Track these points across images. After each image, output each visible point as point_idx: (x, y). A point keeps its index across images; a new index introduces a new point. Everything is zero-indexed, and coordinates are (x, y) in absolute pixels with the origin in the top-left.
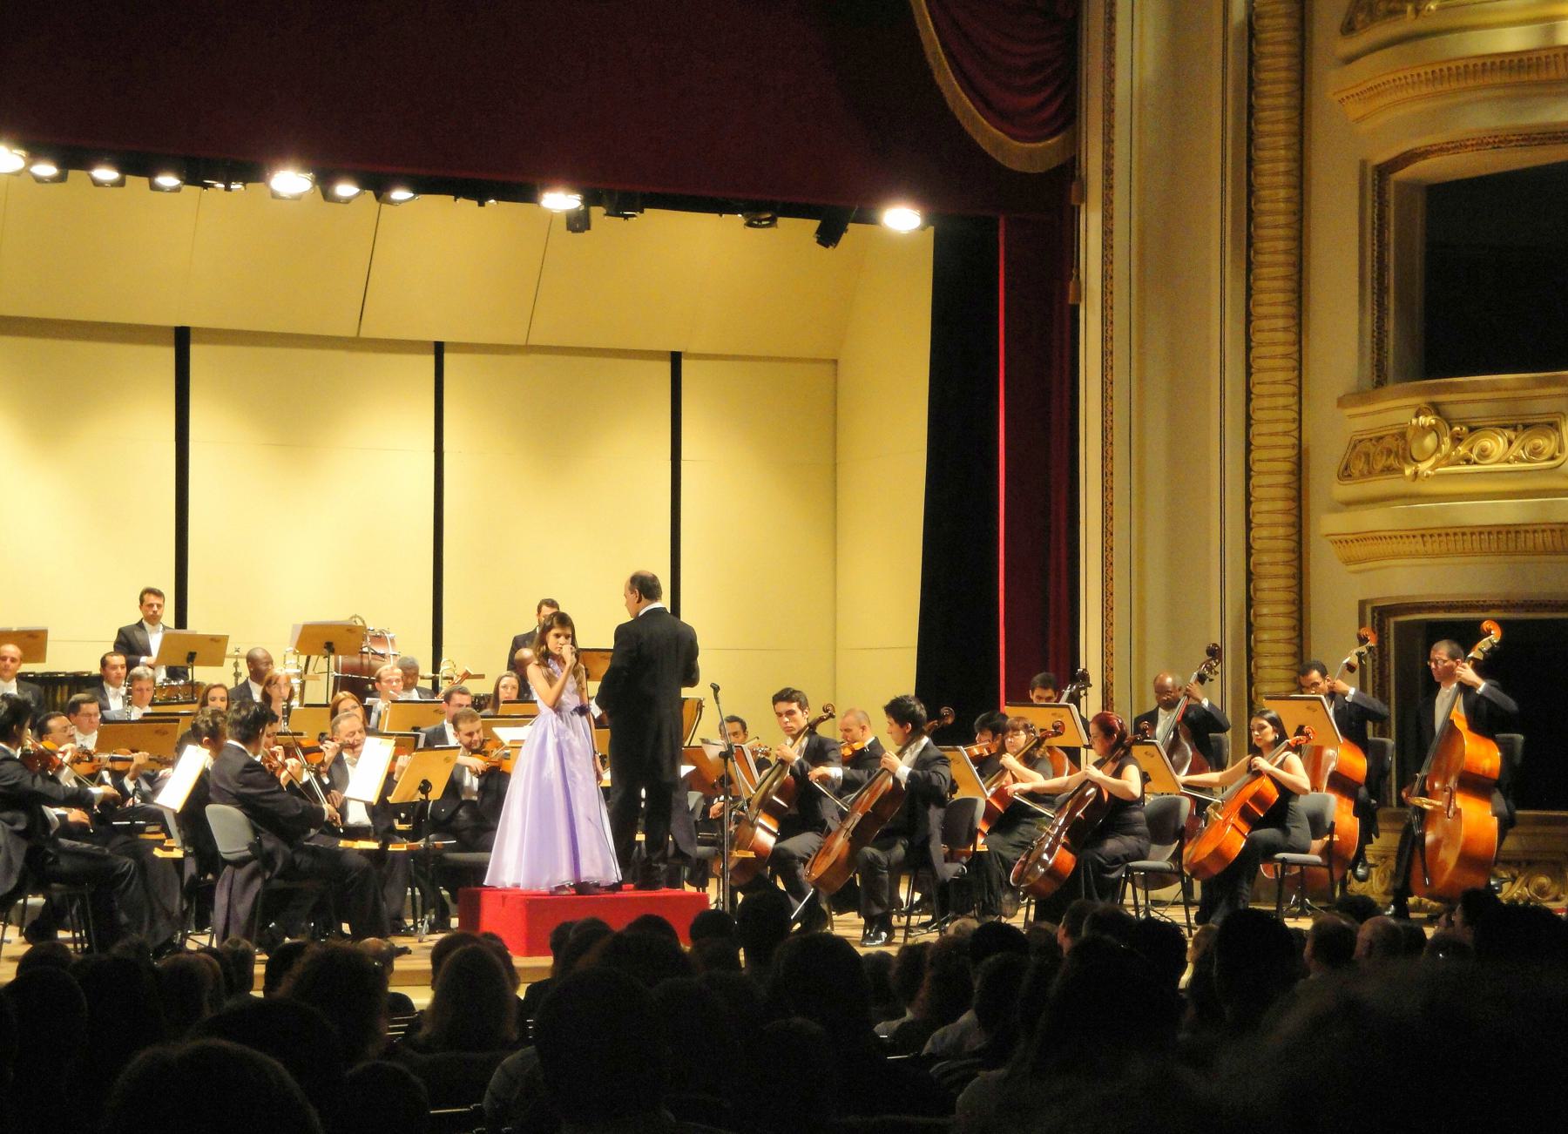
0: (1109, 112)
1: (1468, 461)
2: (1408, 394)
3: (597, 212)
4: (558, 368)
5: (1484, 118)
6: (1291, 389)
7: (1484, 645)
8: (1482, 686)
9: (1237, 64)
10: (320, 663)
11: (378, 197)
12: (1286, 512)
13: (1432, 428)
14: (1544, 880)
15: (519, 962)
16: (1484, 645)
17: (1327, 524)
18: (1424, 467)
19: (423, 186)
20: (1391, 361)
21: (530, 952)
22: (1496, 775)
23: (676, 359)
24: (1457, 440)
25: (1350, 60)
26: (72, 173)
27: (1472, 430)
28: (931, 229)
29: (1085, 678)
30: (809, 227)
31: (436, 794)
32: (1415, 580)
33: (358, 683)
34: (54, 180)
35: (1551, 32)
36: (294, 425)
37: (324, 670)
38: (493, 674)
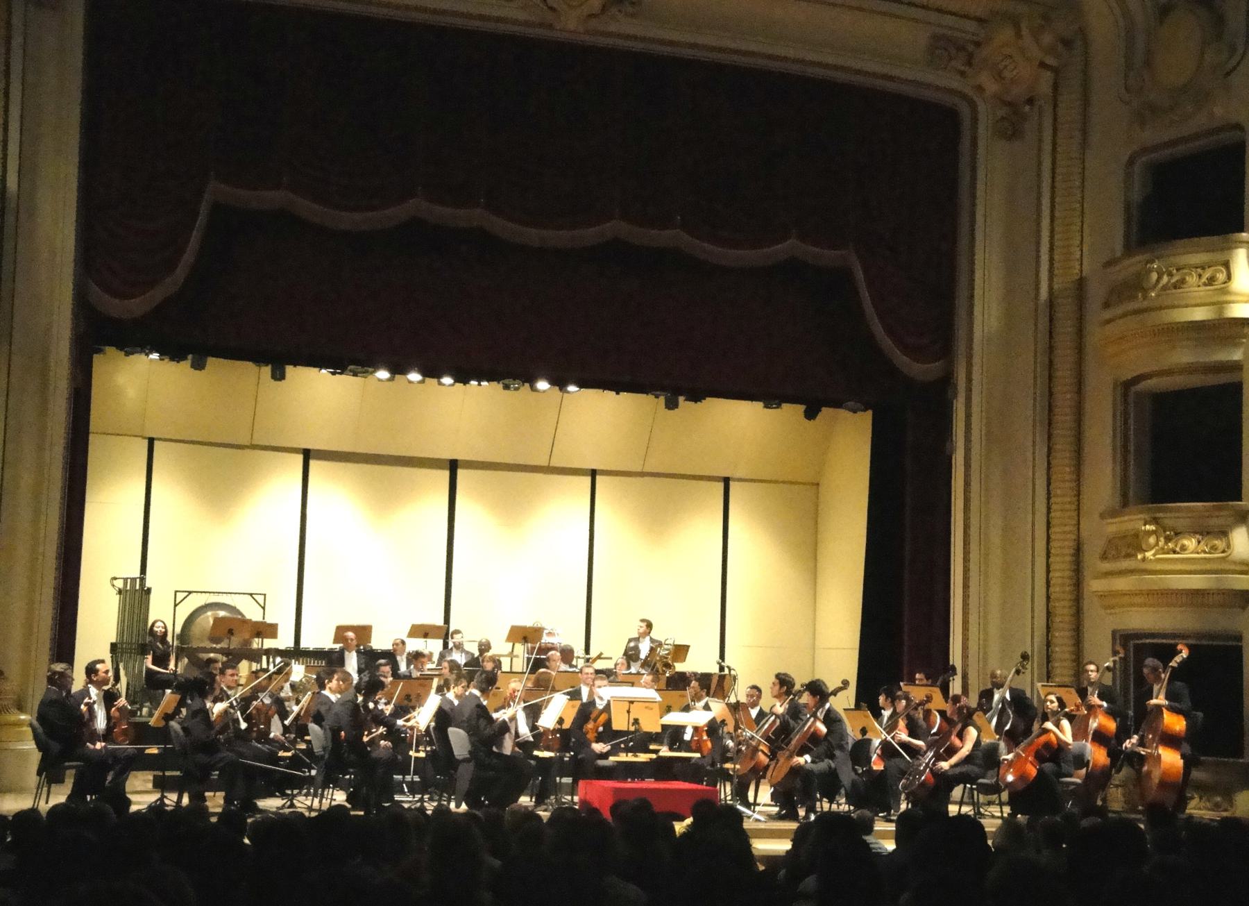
1: (1175, 552)
2: (1141, 513)
5: (1184, 356)
6: (1074, 507)
10: (520, 649)
11: (561, 390)
12: (1070, 578)
13: (1153, 532)
14: (1219, 799)
17: (1095, 585)
18: (1149, 554)
19: (583, 384)
22: (1183, 734)
24: (1168, 539)
25: (1109, 321)
26: (397, 377)
27: (1176, 534)
29: (954, 669)
30: (801, 408)
32: (1142, 620)
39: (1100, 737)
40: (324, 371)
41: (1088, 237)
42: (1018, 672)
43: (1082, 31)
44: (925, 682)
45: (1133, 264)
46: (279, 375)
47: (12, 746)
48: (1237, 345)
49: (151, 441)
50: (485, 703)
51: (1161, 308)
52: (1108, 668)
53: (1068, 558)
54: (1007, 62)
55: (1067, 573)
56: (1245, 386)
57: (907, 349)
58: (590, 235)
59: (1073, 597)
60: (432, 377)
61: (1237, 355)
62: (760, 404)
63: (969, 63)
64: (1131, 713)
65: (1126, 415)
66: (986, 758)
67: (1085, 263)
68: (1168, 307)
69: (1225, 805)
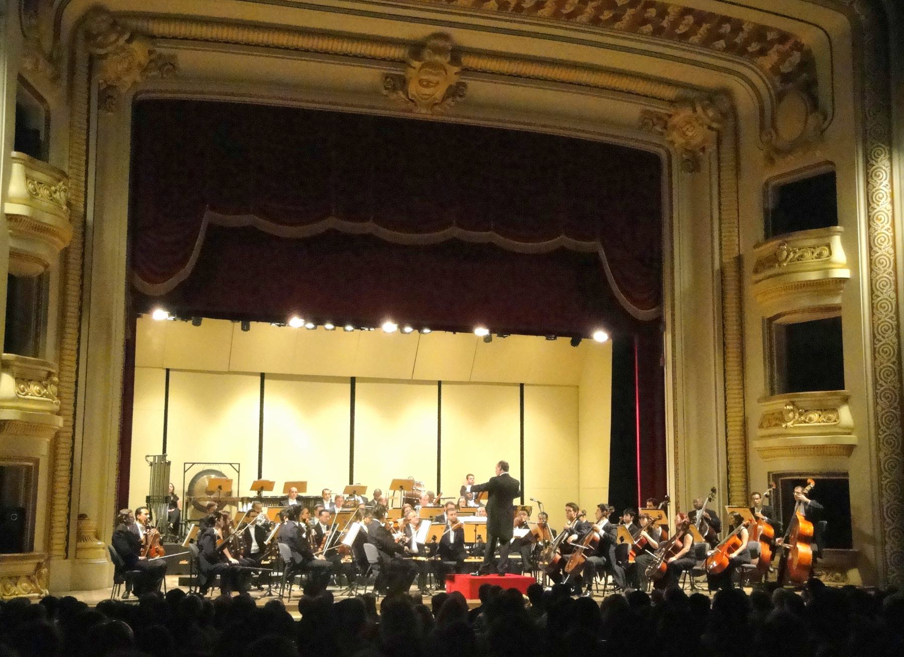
0: (673, 300)
3: (494, 336)
4: (481, 389)
5: (805, 302)
7: (808, 488)
8: (809, 501)
9: (717, 282)
10: (398, 493)
12: (739, 394)
13: (792, 410)
14: (838, 574)
15: (469, 601)
16: (808, 488)
17: (755, 444)
18: (789, 424)
19: (434, 328)
20: (776, 387)
21: (472, 598)
23: (522, 386)
24: (801, 415)
25: (757, 282)
28: (611, 341)
29: (668, 499)
31: (438, 541)
32: (786, 465)
33: (412, 501)
34: (313, 329)
35: (827, 273)
36: (389, 408)
37: (400, 495)
38: (457, 497)
39: (765, 539)
40: (273, 324)
41: (746, 232)
42: (710, 500)
43: (733, 108)
44: (653, 507)
45: (773, 244)
46: (246, 328)
47: (93, 561)
48: (838, 295)
49: (168, 370)
50: (383, 525)
51: (789, 273)
52: (766, 496)
53: (738, 428)
54: (688, 126)
55: (741, 484)
56: (844, 322)
57: (635, 302)
58: (438, 236)
59: (743, 489)
60: (340, 326)
61: (838, 301)
62: (544, 337)
63: (665, 128)
64: (782, 523)
65: (770, 339)
66: (699, 553)
67: (741, 246)
68: (793, 272)
69: (842, 579)
